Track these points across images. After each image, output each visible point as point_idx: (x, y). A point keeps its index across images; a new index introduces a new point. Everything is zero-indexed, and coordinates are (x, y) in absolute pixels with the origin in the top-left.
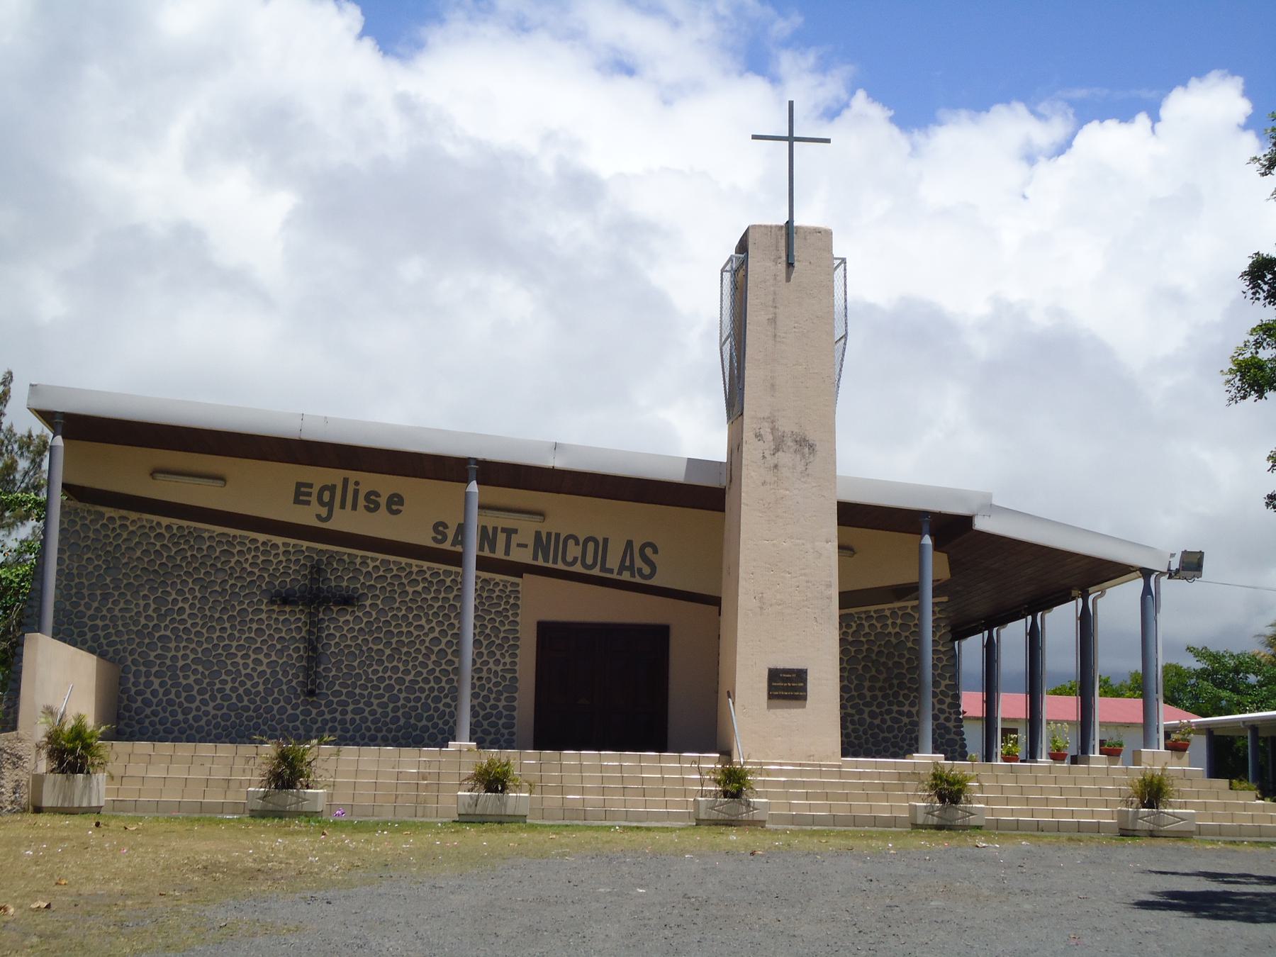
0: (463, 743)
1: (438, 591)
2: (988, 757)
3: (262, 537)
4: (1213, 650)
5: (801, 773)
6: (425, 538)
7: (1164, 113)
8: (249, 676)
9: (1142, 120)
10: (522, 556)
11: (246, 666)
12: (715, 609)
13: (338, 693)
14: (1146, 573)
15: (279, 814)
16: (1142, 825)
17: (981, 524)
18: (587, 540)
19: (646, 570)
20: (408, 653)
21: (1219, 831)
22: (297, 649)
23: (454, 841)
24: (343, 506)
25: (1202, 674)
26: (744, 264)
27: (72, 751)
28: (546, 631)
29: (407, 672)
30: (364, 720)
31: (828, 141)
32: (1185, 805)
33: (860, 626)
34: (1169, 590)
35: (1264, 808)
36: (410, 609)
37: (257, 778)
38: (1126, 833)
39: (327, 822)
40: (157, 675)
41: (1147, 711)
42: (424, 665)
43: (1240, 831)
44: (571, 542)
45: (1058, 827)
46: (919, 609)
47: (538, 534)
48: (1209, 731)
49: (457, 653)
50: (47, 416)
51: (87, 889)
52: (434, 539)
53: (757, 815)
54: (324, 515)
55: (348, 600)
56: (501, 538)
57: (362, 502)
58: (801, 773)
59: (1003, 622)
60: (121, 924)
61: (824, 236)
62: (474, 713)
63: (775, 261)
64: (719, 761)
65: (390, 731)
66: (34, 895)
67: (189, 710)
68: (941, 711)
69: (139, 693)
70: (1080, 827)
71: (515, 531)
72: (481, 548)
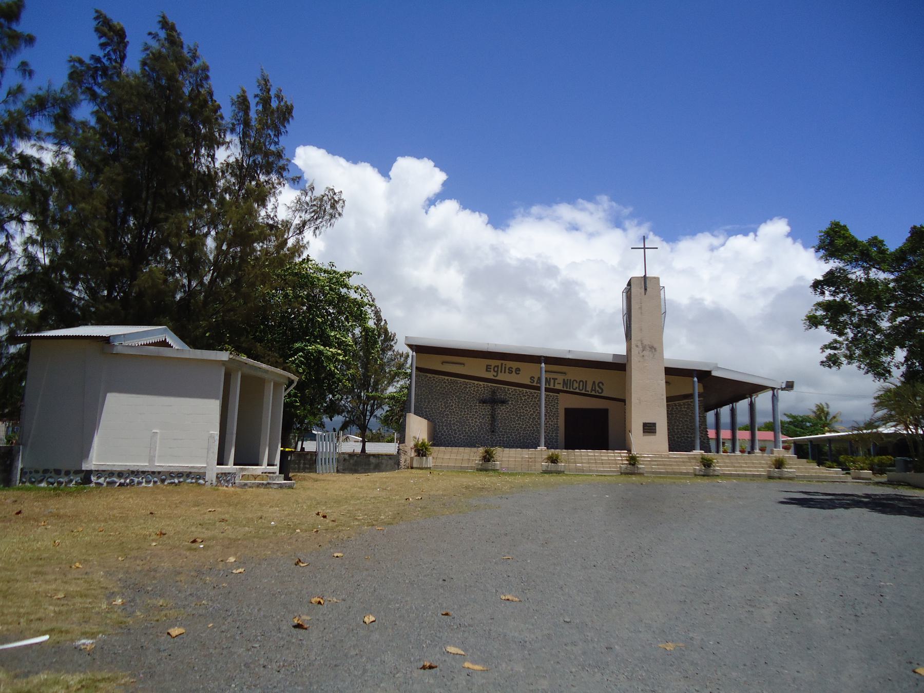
0: (542, 448)
1: (532, 399)
2: (718, 452)
3: (476, 382)
4: (793, 414)
5: (655, 457)
6: (527, 382)
7: (758, 233)
8: (473, 426)
9: (752, 235)
10: (558, 387)
11: (472, 423)
12: (623, 403)
13: (501, 432)
14: (773, 389)
15: (486, 470)
16: (776, 475)
17: (714, 373)
18: (580, 381)
19: (600, 391)
20: (523, 419)
21: (804, 477)
22: (488, 418)
23: (542, 479)
24: (501, 372)
25: (790, 423)
26: (630, 289)
27: (422, 450)
28: (568, 411)
29: (523, 425)
30: (510, 440)
31: (657, 248)
32: (791, 468)
33: (673, 408)
34: (782, 394)
35: (820, 469)
36: (523, 405)
37: (478, 458)
38: (770, 477)
39: (501, 473)
40: (445, 426)
41: (775, 436)
42: (528, 422)
43: (811, 477)
44: (575, 382)
45: (746, 476)
46: (694, 402)
47: (564, 380)
48: (795, 442)
49: (539, 418)
50: (410, 346)
51: (432, 493)
52: (531, 382)
53: (641, 471)
54: (495, 375)
55: (503, 402)
56: (552, 381)
57: (507, 371)
58: (655, 457)
59: (721, 406)
60: (444, 504)
61: (657, 279)
62: (545, 438)
63: (641, 288)
64: (627, 453)
65: (518, 443)
66: (417, 494)
67: (455, 437)
68: (702, 436)
69: (440, 432)
70: (754, 476)
71: (557, 379)
72: (546, 385)
